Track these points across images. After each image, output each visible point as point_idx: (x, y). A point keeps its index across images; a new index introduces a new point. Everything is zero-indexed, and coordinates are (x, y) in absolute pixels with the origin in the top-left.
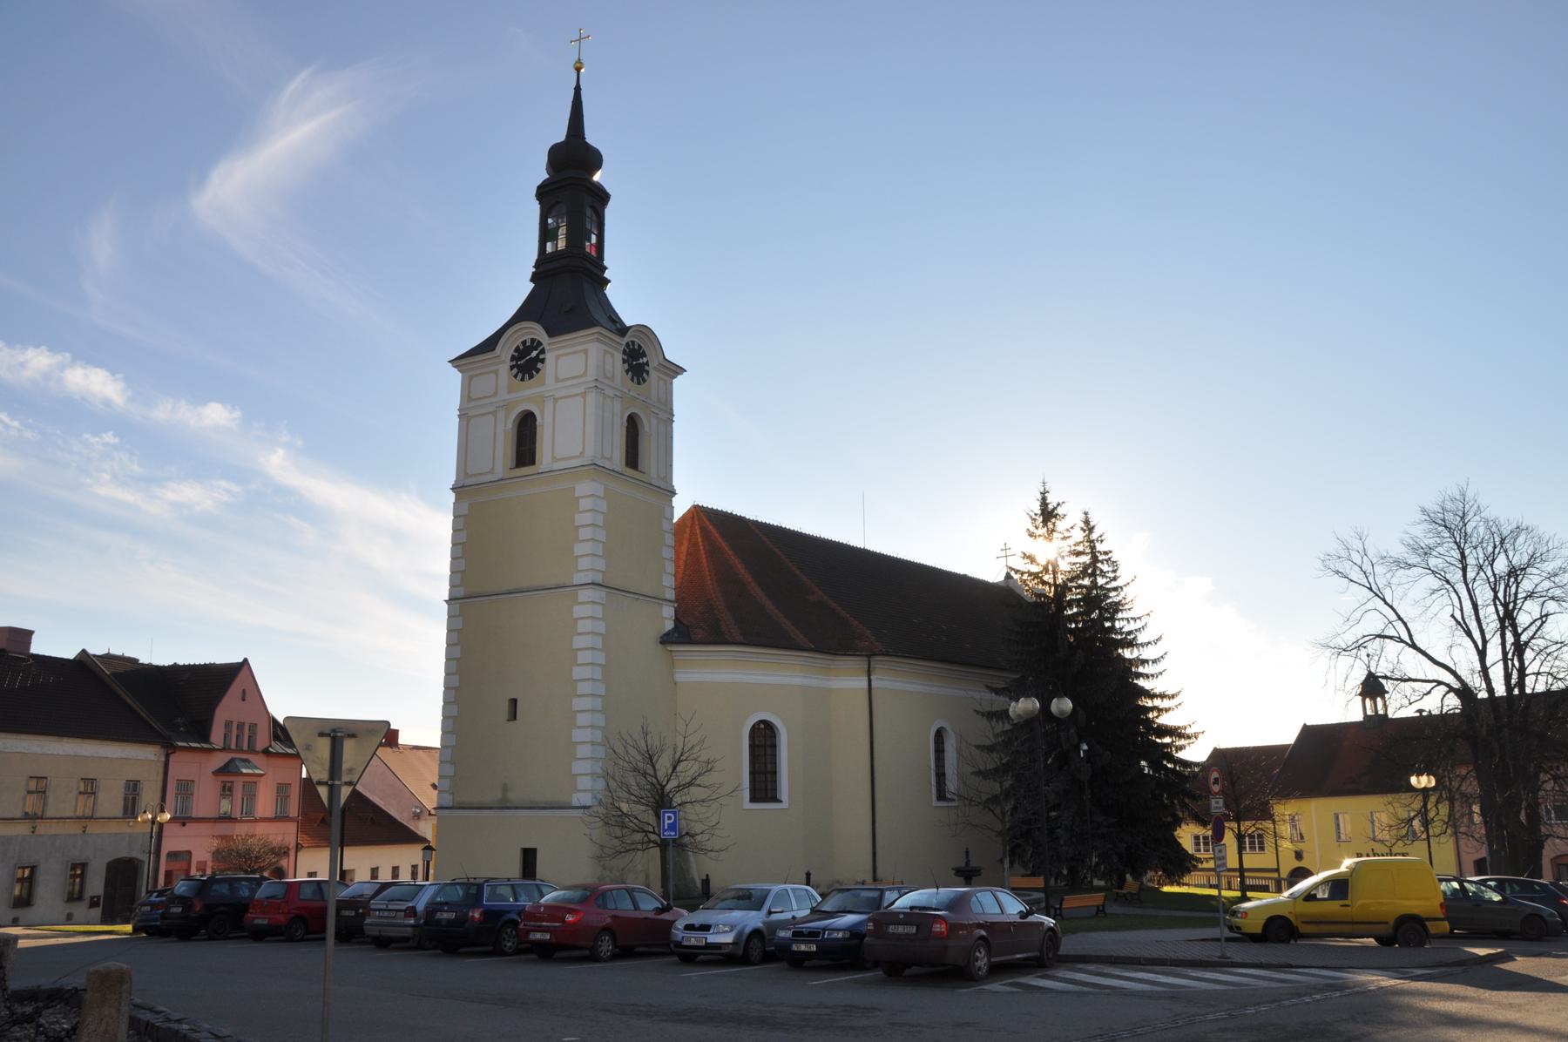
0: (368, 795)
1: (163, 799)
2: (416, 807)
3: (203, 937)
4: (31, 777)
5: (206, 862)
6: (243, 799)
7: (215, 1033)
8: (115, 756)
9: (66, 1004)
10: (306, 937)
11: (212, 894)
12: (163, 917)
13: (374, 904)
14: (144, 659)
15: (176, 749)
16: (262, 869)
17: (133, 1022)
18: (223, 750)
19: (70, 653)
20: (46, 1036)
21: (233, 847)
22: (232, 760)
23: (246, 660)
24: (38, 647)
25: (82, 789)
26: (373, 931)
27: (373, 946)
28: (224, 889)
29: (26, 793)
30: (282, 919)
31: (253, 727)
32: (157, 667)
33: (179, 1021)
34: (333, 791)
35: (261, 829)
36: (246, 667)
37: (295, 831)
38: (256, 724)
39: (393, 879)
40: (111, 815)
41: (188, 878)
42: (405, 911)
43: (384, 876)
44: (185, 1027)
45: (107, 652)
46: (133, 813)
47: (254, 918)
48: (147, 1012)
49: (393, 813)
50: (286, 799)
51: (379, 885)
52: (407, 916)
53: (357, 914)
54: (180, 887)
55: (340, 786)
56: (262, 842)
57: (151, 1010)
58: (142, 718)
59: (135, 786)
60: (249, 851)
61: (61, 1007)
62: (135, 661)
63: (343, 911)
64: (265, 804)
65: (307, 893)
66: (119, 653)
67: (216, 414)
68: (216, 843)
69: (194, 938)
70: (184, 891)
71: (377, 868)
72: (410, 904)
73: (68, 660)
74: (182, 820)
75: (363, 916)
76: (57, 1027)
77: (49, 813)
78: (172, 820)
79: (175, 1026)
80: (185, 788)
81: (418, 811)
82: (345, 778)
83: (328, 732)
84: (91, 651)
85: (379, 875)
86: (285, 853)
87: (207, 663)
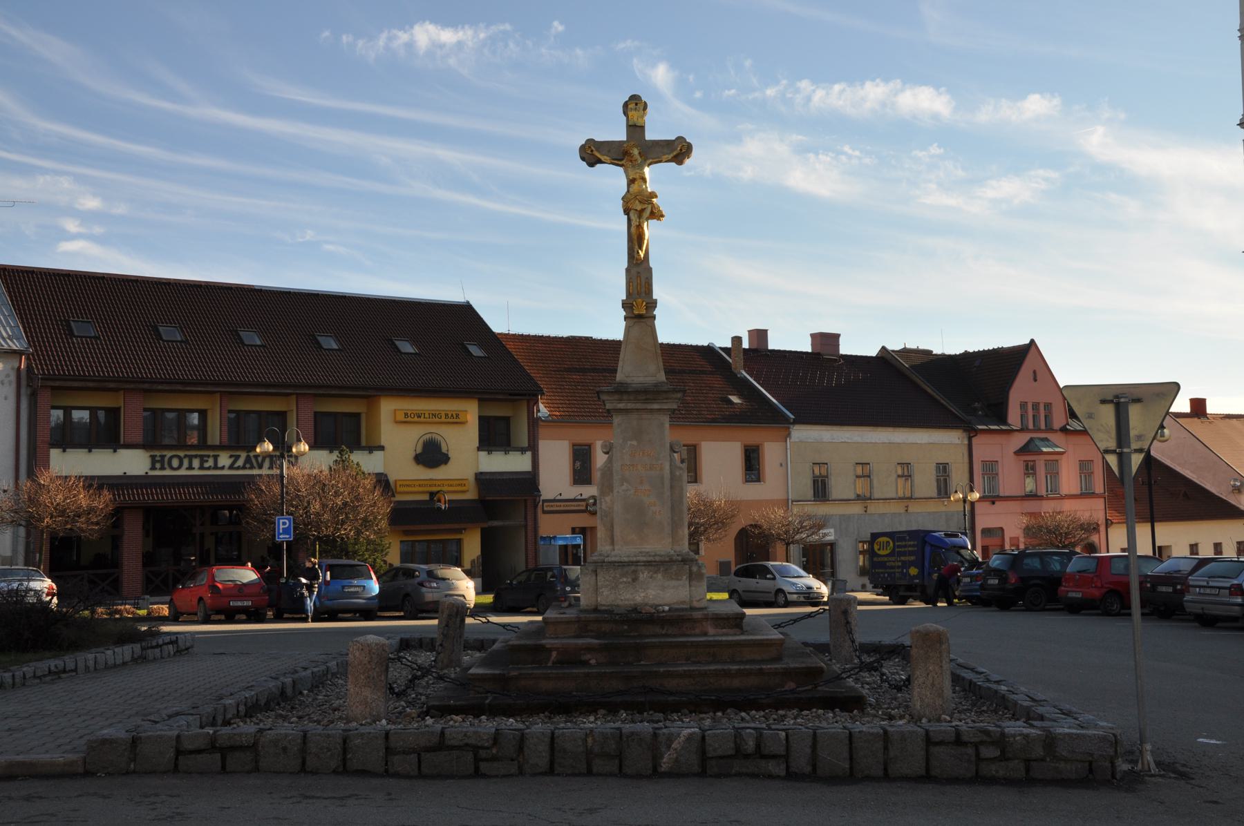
0: (1178, 469)
1: (971, 479)
2: (1235, 480)
3: (1020, 608)
4: (857, 464)
5: (1018, 538)
6: (1047, 477)
7: (1031, 695)
8: (923, 442)
9: (903, 659)
10: (1123, 611)
11: (1025, 567)
12: (982, 587)
13: (1192, 580)
14: (937, 350)
15: (977, 432)
16: (1074, 545)
17: (956, 679)
18: (1023, 430)
19: (872, 351)
20: (889, 684)
21: (1042, 523)
22: (1032, 440)
23: (1032, 341)
24: (846, 349)
25: (900, 472)
26: (1197, 609)
27: (1197, 624)
28: (1036, 563)
29: (854, 477)
30: (1096, 593)
31: (1048, 406)
32: (950, 356)
33: (998, 682)
34: (1123, 459)
35: (1068, 506)
36: (1033, 348)
37: (1103, 507)
38: (1051, 404)
39: (1215, 554)
40: (929, 496)
41: (1002, 552)
42: (1229, 588)
43: (1206, 552)
44: (1003, 688)
45: (903, 347)
46: (946, 493)
47: (1068, 592)
48: (969, 671)
49: (1208, 487)
50: (1090, 476)
51: (1197, 561)
52: (1231, 594)
53: (1175, 591)
54: (995, 561)
55: (1130, 454)
56: (1070, 518)
57: (972, 670)
58: (942, 405)
59: (945, 468)
60: (1058, 527)
61: (899, 661)
62: (929, 353)
63: (1159, 587)
64: (1069, 481)
65: (1118, 568)
66: (913, 346)
67: (1036, 105)
68: (1025, 520)
69: (1013, 608)
70: (998, 565)
71: (1196, 545)
72: (1235, 582)
73: (872, 357)
74: (991, 498)
75: (1182, 593)
76: (897, 677)
77: (876, 495)
78: (981, 499)
79: (994, 686)
80: (991, 468)
81: (1238, 484)
82: (1134, 446)
83: (1110, 398)
84: (890, 347)
85: (1224, 551)
86: (1094, 528)
87: (996, 347)
